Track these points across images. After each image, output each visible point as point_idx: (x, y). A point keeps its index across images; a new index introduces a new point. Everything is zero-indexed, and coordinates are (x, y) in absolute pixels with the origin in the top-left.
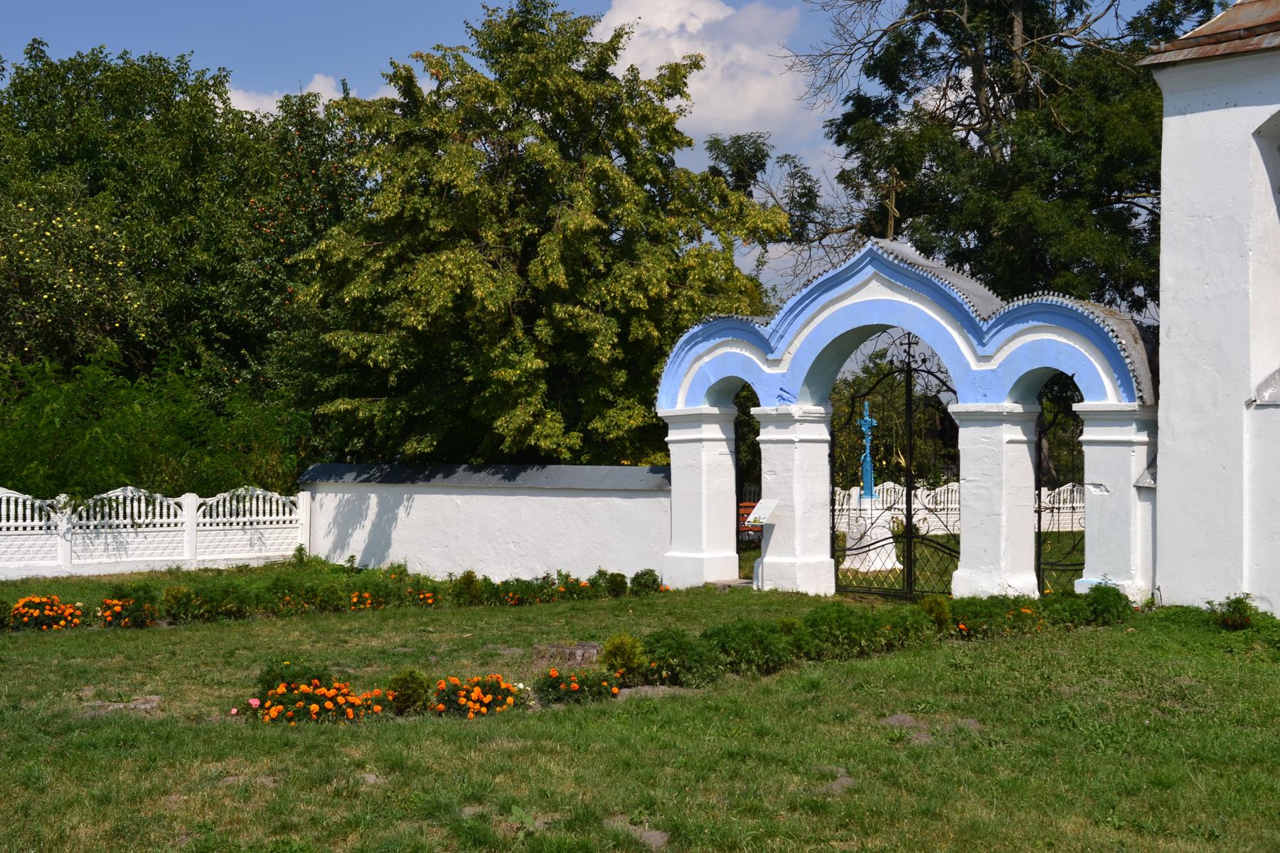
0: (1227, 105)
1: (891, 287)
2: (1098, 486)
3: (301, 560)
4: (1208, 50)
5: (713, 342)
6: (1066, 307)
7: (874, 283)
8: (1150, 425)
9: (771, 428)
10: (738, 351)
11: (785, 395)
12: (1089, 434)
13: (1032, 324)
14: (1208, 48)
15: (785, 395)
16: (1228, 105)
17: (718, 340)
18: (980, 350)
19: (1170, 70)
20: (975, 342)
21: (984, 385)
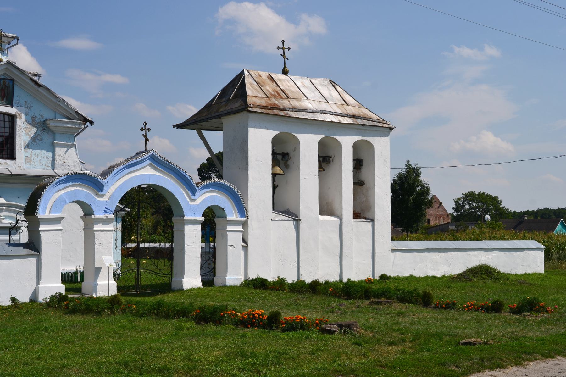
0: (265, 128)
1: (156, 169)
2: (230, 246)
3: (16, 304)
4: (268, 111)
5: (68, 184)
6: (226, 185)
7: (148, 167)
8: (245, 224)
9: (100, 225)
10: (81, 189)
11: (107, 211)
12: (42, 227)
13: (211, 189)
14: (11, 69)
15: (107, 211)
16: (265, 128)
17: (71, 183)
18: (193, 197)
19: (254, 114)
20: (190, 194)
21: (193, 210)
